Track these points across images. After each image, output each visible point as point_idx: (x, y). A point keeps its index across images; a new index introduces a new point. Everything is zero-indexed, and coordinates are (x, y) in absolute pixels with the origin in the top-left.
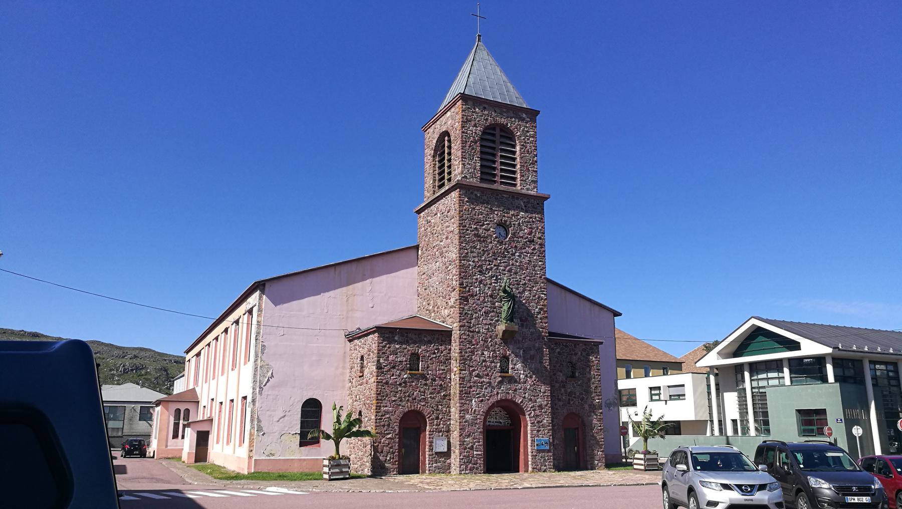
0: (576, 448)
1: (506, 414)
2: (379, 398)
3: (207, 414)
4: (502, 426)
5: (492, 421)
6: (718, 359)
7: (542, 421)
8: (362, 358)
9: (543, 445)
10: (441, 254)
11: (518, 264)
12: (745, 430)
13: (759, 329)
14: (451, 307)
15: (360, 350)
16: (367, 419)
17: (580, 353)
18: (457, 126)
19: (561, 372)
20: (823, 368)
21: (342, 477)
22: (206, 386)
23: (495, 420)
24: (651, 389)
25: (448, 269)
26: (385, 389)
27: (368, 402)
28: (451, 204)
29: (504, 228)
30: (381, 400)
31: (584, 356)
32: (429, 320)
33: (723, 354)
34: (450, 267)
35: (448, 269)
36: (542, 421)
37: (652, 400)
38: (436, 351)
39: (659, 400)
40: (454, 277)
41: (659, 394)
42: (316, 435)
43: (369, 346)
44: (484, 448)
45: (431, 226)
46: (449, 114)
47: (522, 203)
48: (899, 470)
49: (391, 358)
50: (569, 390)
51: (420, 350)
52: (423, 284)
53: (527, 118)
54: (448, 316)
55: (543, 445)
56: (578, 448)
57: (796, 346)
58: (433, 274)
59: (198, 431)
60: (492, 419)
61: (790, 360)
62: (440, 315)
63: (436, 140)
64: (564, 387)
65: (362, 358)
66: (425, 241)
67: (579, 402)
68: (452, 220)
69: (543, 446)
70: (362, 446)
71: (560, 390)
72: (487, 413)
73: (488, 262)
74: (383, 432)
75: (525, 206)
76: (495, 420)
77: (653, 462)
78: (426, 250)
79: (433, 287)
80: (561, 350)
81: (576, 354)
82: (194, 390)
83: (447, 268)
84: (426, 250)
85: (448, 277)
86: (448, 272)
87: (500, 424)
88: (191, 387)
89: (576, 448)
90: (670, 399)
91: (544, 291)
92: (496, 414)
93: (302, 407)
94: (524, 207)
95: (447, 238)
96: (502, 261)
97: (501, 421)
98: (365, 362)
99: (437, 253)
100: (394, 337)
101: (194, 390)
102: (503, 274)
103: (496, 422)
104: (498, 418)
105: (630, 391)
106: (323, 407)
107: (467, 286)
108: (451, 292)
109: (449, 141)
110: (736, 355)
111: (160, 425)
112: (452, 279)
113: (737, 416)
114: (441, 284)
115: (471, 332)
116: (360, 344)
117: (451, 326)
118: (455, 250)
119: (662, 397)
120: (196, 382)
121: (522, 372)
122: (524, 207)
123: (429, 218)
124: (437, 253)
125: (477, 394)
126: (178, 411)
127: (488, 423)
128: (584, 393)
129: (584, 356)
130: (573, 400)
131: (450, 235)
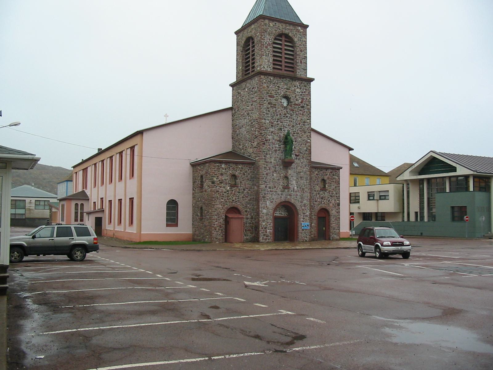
0: (324, 228)
1: (285, 209)
3: (98, 207)
4: (283, 216)
5: (277, 214)
6: (409, 176)
8: (202, 176)
10: (248, 114)
11: (294, 121)
12: (422, 218)
13: (434, 158)
14: (255, 147)
15: (200, 172)
16: (206, 212)
17: (329, 174)
18: (259, 35)
19: (318, 185)
20: (468, 183)
21: (439, 258)
22: (95, 190)
24: (368, 192)
25: (253, 124)
27: (206, 202)
28: (255, 84)
29: (288, 102)
32: (249, 157)
33: (413, 172)
34: (254, 123)
35: (253, 124)
37: (369, 199)
38: (246, 174)
39: (373, 199)
40: (257, 129)
41: (374, 196)
42: (363, 250)
43: (206, 170)
44: (273, 228)
45: (240, 96)
46: (253, 26)
47: (298, 84)
49: (220, 177)
52: (235, 132)
53: (302, 29)
54: (253, 153)
56: (325, 229)
57: (454, 169)
58: (243, 126)
59: (95, 217)
61: (450, 177)
62: (247, 152)
63: (244, 41)
64: (319, 194)
65: (202, 176)
66: (237, 104)
68: (256, 94)
70: (203, 226)
71: (317, 196)
72: (275, 210)
78: (238, 111)
79: (242, 134)
82: (83, 192)
83: (252, 123)
84: (238, 111)
85: (252, 129)
86: (252, 126)
87: (282, 215)
88: (80, 189)
89: (324, 228)
90: (380, 199)
93: (167, 205)
94: (299, 86)
95: (252, 105)
97: (282, 213)
98: (204, 179)
99: (245, 113)
100: (221, 165)
101: (83, 192)
103: (279, 214)
104: (280, 211)
105: (356, 193)
108: (255, 139)
109: (253, 43)
110: (420, 174)
111: (468, 265)
112: (255, 131)
113: (418, 210)
114: (248, 133)
116: (200, 168)
117: (254, 159)
118: (258, 113)
119: (375, 198)
120: (85, 185)
122: (299, 86)
123: (239, 91)
124: (245, 113)
125: (270, 198)
126: (77, 205)
127: (275, 215)
128: (330, 197)
131: (254, 104)
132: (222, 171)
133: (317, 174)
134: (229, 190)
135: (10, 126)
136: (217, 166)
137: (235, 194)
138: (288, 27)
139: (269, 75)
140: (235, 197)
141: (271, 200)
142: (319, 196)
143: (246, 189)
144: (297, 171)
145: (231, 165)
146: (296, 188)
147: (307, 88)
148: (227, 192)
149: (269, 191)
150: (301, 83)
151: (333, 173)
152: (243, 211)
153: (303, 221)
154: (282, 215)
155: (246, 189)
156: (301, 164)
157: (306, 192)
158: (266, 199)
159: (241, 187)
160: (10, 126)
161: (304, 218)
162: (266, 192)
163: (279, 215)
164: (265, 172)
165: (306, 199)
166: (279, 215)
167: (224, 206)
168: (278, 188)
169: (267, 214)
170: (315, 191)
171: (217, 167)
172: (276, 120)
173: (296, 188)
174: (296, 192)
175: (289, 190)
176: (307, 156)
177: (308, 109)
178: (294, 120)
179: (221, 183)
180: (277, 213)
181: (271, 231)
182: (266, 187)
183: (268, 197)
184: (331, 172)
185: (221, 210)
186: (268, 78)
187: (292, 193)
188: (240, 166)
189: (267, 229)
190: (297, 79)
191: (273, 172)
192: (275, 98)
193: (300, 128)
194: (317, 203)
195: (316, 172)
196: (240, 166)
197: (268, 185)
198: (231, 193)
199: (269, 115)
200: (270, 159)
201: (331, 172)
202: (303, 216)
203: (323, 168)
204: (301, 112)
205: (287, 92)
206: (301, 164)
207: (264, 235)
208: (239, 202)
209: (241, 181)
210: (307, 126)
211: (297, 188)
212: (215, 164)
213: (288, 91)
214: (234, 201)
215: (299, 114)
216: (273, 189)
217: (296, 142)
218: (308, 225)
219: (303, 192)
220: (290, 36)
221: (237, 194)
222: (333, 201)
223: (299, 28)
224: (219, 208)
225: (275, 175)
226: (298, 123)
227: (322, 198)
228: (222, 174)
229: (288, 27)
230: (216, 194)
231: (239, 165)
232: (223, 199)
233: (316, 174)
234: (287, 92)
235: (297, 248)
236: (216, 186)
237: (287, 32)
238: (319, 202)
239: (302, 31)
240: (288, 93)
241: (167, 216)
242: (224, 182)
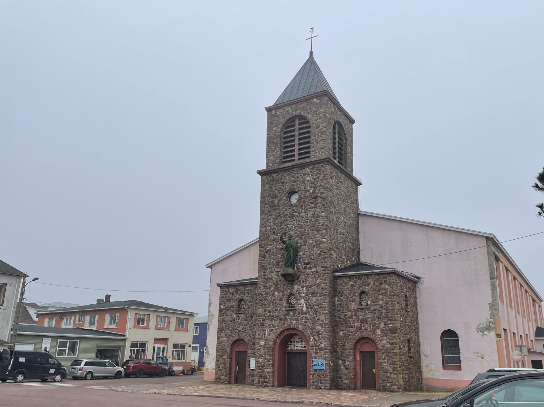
2: (220, 331)
7: (320, 345)
9: (319, 365)
23: (301, 345)
26: (222, 325)
30: (220, 333)
31: (377, 286)
36: (320, 345)
38: (254, 296)
48: (7, 373)
50: (361, 317)
51: (244, 297)
53: (318, 100)
55: (319, 365)
60: (299, 344)
64: (355, 315)
67: (370, 328)
69: (320, 367)
73: (280, 224)
74: (221, 354)
75: (311, 172)
76: (301, 345)
77: (474, 392)
80: (354, 282)
81: (368, 285)
87: (305, 349)
91: (325, 236)
92: (302, 340)
94: (310, 173)
96: (291, 220)
102: (291, 230)
105: (148, 321)
106: (460, 339)
107: (264, 245)
115: (266, 279)
121: (304, 305)
122: (310, 173)
129: (377, 286)
130: (364, 326)
132: (229, 296)
133: (352, 286)
134: (235, 318)
135: (34, 280)
136: (225, 291)
137: (241, 323)
138: (299, 106)
139: (272, 173)
140: (242, 326)
141: (270, 327)
142: (357, 318)
143: (254, 316)
144: (307, 284)
145: (239, 287)
146: (305, 309)
147: (321, 172)
148: (233, 321)
149: (268, 315)
150: (314, 168)
151: (380, 281)
152: (250, 344)
153: (315, 358)
154: (305, 349)
155: (254, 316)
156: (313, 274)
157: (320, 313)
158: (264, 326)
159: (249, 313)
160: (34, 280)
161: (316, 353)
162: (265, 318)
163: (302, 348)
164: (264, 291)
165: (320, 324)
166: (302, 348)
167: (229, 338)
168: (280, 310)
169: (265, 347)
170: (350, 311)
171: (225, 292)
172: (280, 224)
173: (305, 309)
174: (306, 313)
175: (295, 312)
176: (322, 262)
177: (322, 198)
178: (302, 217)
179: (228, 310)
180: (299, 345)
181: (269, 370)
182: (265, 311)
183: (267, 323)
184: (377, 280)
185: (226, 343)
186: (270, 177)
187: (300, 316)
188: (248, 288)
189: (265, 368)
190: (307, 165)
191: (274, 291)
192: (278, 198)
193: (311, 227)
194: (353, 330)
195: (351, 283)
196: (248, 288)
197: (267, 308)
198: (238, 322)
199: (271, 221)
200: (271, 274)
201: (377, 280)
202: (316, 350)
203: (363, 275)
204: (313, 205)
205: (293, 185)
206: (313, 274)
207: (261, 376)
208: (245, 332)
209: (249, 306)
210: (321, 222)
211: (307, 308)
212: (223, 290)
213: (295, 184)
214: (240, 331)
215: (309, 209)
216: (273, 312)
217: (305, 245)
218: (322, 364)
219: (316, 313)
220: (290, 118)
221: (244, 323)
222: (382, 326)
223: (315, 100)
224: (223, 341)
225: (276, 293)
226: (308, 221)
227: (362, 321)
228: (229, 300)
229: (299, 106)
230: (222, 324)
231: (248, 287)
232: (228, 330)
233: (350, 286)
234: (293, 185)
235: (248, 395)
236: (223, 314)
237: (298, 112)
238: (357, 327)
239: (319, 101)
240: (295, 186)
241: (460, 356)
242: (231, 309)
